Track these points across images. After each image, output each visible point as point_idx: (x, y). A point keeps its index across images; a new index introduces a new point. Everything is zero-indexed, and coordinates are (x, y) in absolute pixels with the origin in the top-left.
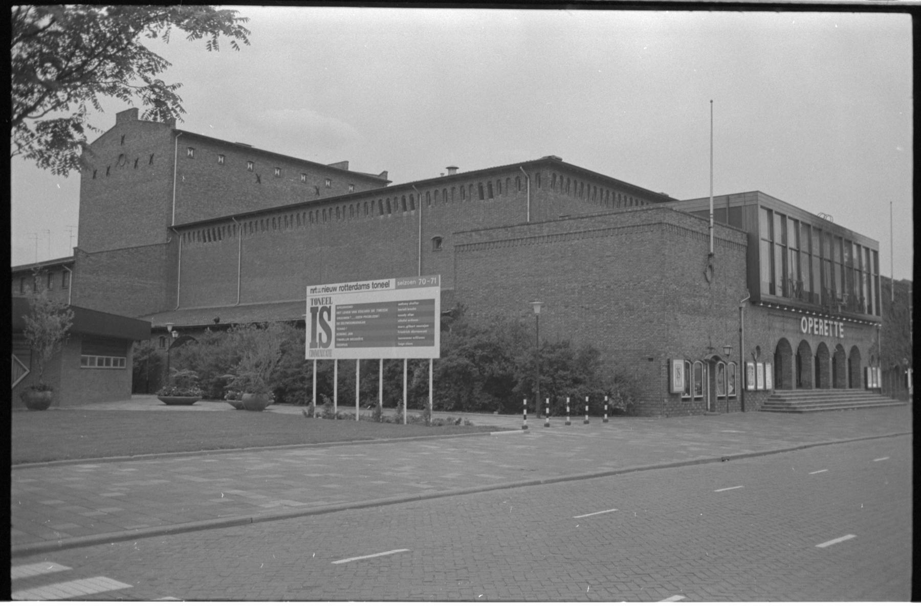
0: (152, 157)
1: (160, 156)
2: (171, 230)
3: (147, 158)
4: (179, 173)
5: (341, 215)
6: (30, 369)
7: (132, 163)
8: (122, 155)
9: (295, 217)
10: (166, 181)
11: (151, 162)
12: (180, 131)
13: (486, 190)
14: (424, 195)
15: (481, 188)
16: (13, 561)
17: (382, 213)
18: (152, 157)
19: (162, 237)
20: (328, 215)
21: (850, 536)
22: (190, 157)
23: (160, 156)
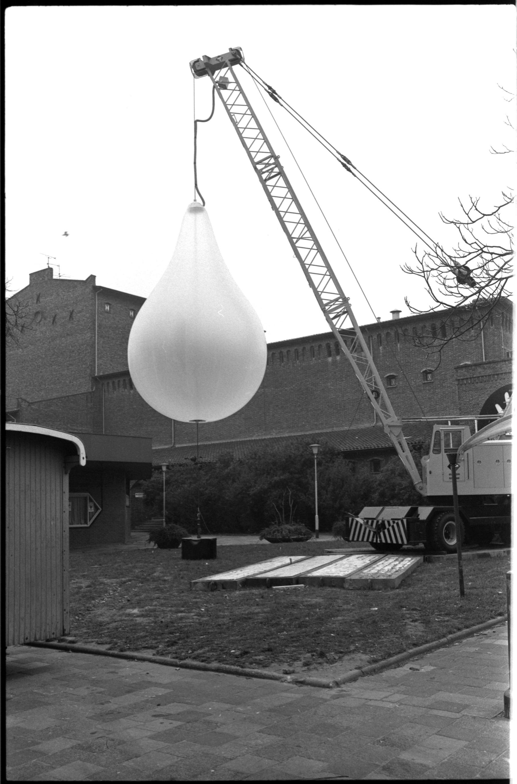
0: (71, 313)
1: (80, 312)
2: (97, 380)
3: (66, 314)
4: (100, 326)
5: (285, 359)
6: (102, 508)
7: (50, 320)
8: (37, 313)
9: (111, 384)
10: (89, 335)
11: (71, 316)
12: (100, 287)
13: (439, 331)
14: (375, 337)
15: (434, 328)
16: (7, 678)
17: (330, 355)
18: (71, 313)
19: (86, 387)
20: (117, 386)
21: (274, 587)
22: (107, 312)
23: (80, 312)
